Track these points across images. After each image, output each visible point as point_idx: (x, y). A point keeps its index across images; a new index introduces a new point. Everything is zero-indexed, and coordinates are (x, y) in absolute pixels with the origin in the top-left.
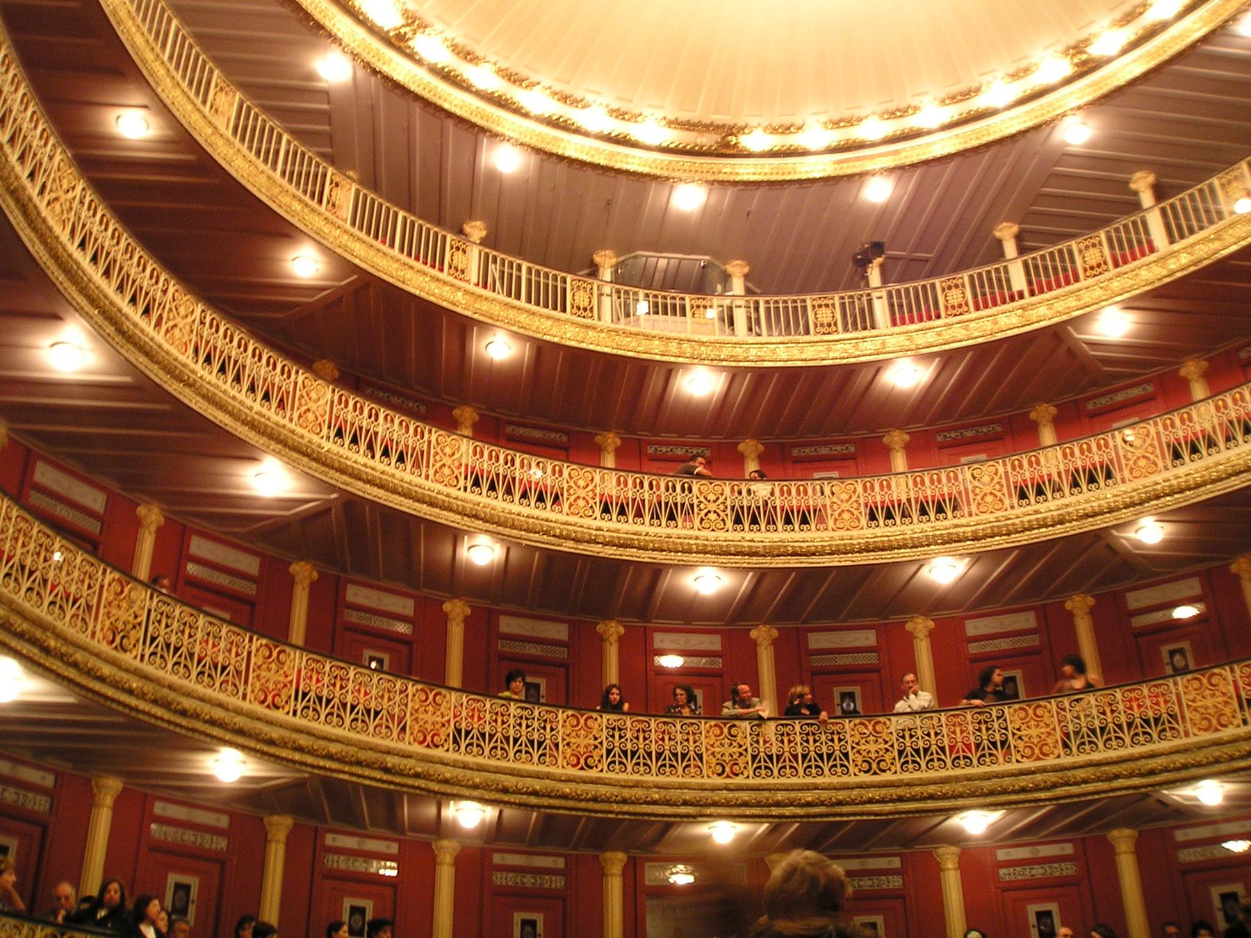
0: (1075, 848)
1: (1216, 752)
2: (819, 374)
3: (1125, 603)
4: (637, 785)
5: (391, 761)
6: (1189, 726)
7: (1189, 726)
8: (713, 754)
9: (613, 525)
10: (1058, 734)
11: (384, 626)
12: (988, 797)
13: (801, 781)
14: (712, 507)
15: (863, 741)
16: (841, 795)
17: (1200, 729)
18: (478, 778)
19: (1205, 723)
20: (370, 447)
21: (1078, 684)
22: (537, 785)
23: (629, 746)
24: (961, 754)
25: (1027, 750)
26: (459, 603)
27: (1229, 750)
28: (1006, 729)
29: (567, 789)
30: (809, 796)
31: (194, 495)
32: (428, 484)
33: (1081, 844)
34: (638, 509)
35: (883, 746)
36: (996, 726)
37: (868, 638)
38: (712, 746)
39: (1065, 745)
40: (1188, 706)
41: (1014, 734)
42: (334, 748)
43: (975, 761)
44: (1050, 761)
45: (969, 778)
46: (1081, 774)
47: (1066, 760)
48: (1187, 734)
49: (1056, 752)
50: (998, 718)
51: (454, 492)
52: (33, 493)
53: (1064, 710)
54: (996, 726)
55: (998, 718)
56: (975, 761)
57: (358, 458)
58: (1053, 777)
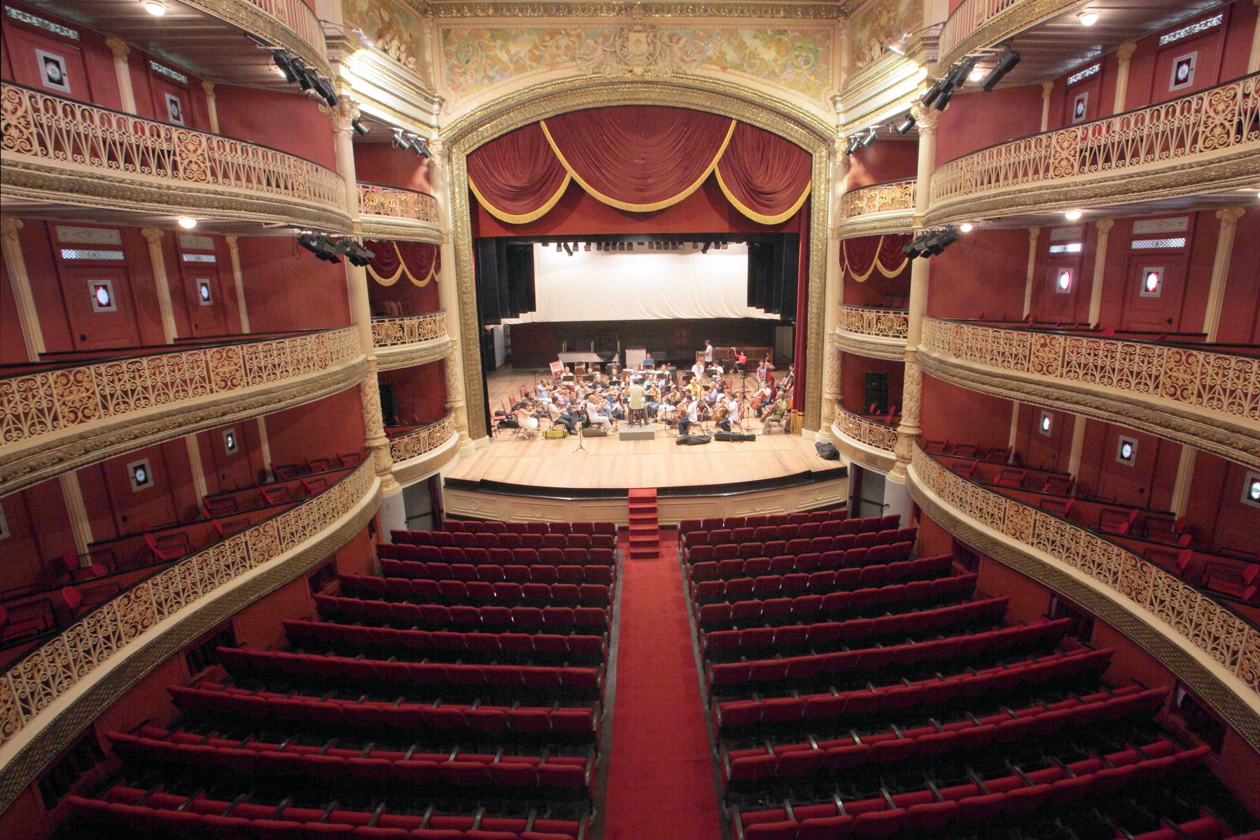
7: (213, 385)
19: (223, 384)
48: (212, 391)
55: (43, 385)
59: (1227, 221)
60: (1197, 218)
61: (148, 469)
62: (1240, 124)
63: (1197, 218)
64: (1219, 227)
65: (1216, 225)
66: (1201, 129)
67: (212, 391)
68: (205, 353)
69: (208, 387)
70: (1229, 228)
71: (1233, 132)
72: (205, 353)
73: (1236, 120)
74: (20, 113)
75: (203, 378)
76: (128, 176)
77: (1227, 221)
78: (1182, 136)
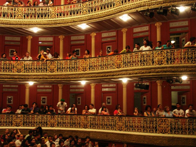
0: (18, 86)
3: (169, 25)
6: (14, 70)
7: (14, 70)
8: (55, 66)
9: (37, 20)
11: (106, 40)
13: (183, 65)
14: (20, 13)
15: (21, 68)
17: (16, 72)
19: (17, 71)
21: (88, 56)
23: (190, 56)
24: (28, 70)
25: (50, 70)
28: (157, 124)
33: (53, 86)
34: (42, 15)
35: (54, 67)
38: (49, 66)
40: (15, 67)
41: (48, 67)
43: (40, 72)
48: (13, 72)
49: (23, 72)
53: (58, 63)
55: (79, 62)
56: (40, 72)
59: (158, 26)
60: (118, 32)
61: (111, 100)
62: (89, 10)
63: (118, 32)
64: (91, 37)
65: (91, 37)
66: (81, 10)
67: (24, 72)
68: (14, 62)
69: (13, 71)
70: (159, 28)
71: (121, 3)
72: (14, 62)
73: (88, 9)
75: (113, 64)
76: (4, 19)
77: (158, 26)
78: (102, 7)
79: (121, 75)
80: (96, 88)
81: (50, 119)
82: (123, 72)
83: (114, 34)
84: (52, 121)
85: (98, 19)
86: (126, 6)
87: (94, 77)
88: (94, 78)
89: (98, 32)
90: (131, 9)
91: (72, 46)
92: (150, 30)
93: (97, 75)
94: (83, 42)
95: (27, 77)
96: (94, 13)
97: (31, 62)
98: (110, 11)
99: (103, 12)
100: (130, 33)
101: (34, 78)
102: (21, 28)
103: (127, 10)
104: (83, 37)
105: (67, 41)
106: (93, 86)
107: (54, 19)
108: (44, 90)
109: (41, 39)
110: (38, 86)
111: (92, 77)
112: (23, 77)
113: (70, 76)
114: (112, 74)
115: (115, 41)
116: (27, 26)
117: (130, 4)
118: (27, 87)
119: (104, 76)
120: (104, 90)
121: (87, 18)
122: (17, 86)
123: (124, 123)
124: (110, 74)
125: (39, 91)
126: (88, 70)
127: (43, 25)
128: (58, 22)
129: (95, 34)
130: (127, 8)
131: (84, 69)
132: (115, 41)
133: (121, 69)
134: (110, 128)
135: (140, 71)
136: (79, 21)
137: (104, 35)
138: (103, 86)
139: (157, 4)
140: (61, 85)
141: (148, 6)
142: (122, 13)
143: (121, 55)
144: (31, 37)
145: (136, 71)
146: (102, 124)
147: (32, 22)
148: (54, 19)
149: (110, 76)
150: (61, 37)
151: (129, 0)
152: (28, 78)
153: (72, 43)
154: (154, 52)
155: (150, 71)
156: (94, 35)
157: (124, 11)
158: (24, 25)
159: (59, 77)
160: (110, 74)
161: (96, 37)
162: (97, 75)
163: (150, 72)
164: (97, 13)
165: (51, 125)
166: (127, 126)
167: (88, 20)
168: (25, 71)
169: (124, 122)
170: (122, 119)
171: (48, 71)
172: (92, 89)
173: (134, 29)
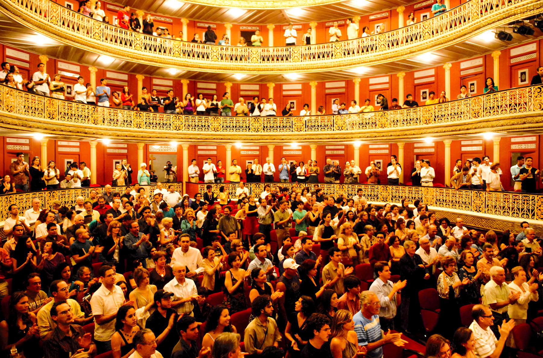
1: (298, 137)
2: (152, 67)
4: (154, 132)
5: (87, 130)
10: (262, 127)
12: (245, 140)
16: (207, 137)
18: (110, 132)
20: (73, 28)
22: (127, 133)
26: (94, 68)
27: (301, 137)
28: (534, 205)
29: (134, 134)
30: (199, 137)
31: (451, 50)
32: (92, 40)
36: (531, 203)
37: (214, 86)
39: (264, 129)
42: (71, 129)
44: (259, 133)
45: (239, 135)
46: (266, 137)
47: (263, 133)
50: (532, 200)
51: (98, 42)
52: (7, 59)
54: (531, 203)
55: (532, 200)
57: (69, 32)
58: (259, 137)
73: (480, 10)
74: (57, 13)
79: (479, 128)
80: (452, 146)
81: (381, 191)
82: (501, 121)
83: (480, 61)
84: (385, 194)
85: (445, 44)
86: (486, 19)
87: (441, 132)
88: (316, 140)
89: (454, 62)
90: (494, 22)
91: (513, 68)
92: (391, 83)
93: (444, 129)
94: (433, 79)
95: (350, 136)
96: (437, 37)
97: (373, 114)
98: (463, 30)
99: (458, 29)
100: (505, 56)
101: (360, 137)
102: (341, 71)
103: (489, 24)
104: (432, 72)
105: (410, 77)
106: (447, 143)
107: (384, 52)
108: (379, 152)
109: (372, 81)
110: (370, 147)
111: (452, 131)
112: (345, 136)
113: (407, 132)
114: (466, 127)
115: (482, 73)
116: (348, 66)
117: (493, 14)
118: (355, 149)
119: (455, 131)
120: (464, 149)
121: (430, 44)
122: (343, 147)
123: (484, 201)
124: (463, 127)
125: (371, 152)
126: (433, 122)
127: (369, 63)
128: (389, 55)
129: (499, 53)
130: (489, 21)
131: (427, 122)
132: (482, 73)
133: (479, 119)
134: (444, 204)
135: (508, 121)
136: (419, 51)
137: (463, 65)
138: (463, 143)
139: (537, 9)
140: (402, 143)
141: (521, 13)
142: (480, 30)
143: (480, 97)
144: (360, 80)
145: (502, 122)
146: (452, 201)
147: (349, 61)
148: (384, 52)
149: (463, 130)
150: (401, 75)
151: (510, 1)
152: (422, 132)
153: (417, 82)
154: (532, 89)
155: (523, 120)
156: (448, 66)
157: (484, 26)
158: (343, 66)
159: (392, 134)
160: (463, 127)
161: (451, 70)
162: (444, 129)
163: (524, 123)
164: (444, 35)
165: (383, 199)
166: (488, 206)
167: (431, 47)
168: (307, 129)
169: (484, 199)
170: (481, 195)
171: (377, 127)
172: (91, 149)
173: (511, 50)
